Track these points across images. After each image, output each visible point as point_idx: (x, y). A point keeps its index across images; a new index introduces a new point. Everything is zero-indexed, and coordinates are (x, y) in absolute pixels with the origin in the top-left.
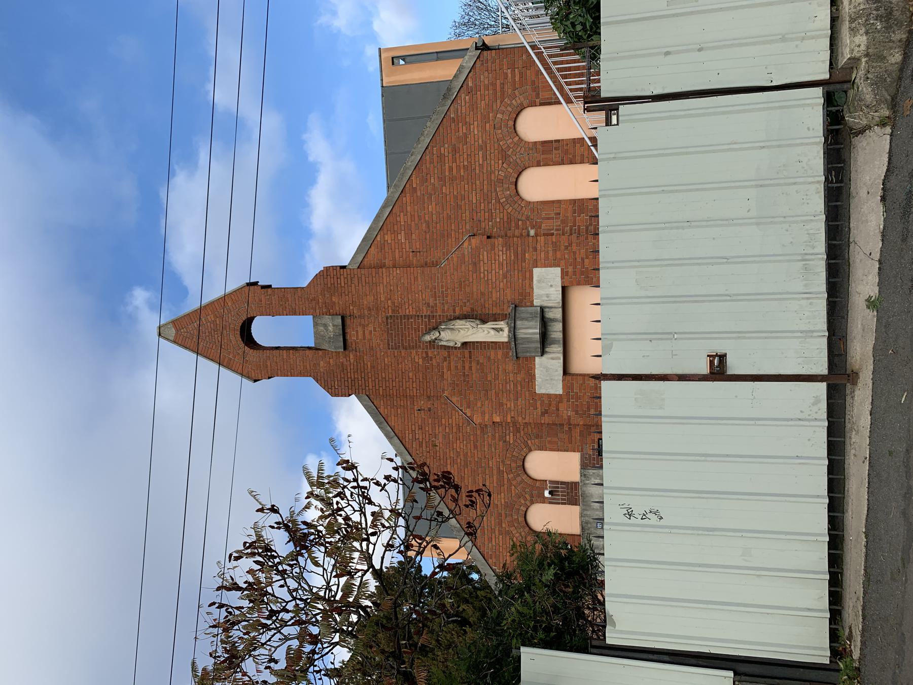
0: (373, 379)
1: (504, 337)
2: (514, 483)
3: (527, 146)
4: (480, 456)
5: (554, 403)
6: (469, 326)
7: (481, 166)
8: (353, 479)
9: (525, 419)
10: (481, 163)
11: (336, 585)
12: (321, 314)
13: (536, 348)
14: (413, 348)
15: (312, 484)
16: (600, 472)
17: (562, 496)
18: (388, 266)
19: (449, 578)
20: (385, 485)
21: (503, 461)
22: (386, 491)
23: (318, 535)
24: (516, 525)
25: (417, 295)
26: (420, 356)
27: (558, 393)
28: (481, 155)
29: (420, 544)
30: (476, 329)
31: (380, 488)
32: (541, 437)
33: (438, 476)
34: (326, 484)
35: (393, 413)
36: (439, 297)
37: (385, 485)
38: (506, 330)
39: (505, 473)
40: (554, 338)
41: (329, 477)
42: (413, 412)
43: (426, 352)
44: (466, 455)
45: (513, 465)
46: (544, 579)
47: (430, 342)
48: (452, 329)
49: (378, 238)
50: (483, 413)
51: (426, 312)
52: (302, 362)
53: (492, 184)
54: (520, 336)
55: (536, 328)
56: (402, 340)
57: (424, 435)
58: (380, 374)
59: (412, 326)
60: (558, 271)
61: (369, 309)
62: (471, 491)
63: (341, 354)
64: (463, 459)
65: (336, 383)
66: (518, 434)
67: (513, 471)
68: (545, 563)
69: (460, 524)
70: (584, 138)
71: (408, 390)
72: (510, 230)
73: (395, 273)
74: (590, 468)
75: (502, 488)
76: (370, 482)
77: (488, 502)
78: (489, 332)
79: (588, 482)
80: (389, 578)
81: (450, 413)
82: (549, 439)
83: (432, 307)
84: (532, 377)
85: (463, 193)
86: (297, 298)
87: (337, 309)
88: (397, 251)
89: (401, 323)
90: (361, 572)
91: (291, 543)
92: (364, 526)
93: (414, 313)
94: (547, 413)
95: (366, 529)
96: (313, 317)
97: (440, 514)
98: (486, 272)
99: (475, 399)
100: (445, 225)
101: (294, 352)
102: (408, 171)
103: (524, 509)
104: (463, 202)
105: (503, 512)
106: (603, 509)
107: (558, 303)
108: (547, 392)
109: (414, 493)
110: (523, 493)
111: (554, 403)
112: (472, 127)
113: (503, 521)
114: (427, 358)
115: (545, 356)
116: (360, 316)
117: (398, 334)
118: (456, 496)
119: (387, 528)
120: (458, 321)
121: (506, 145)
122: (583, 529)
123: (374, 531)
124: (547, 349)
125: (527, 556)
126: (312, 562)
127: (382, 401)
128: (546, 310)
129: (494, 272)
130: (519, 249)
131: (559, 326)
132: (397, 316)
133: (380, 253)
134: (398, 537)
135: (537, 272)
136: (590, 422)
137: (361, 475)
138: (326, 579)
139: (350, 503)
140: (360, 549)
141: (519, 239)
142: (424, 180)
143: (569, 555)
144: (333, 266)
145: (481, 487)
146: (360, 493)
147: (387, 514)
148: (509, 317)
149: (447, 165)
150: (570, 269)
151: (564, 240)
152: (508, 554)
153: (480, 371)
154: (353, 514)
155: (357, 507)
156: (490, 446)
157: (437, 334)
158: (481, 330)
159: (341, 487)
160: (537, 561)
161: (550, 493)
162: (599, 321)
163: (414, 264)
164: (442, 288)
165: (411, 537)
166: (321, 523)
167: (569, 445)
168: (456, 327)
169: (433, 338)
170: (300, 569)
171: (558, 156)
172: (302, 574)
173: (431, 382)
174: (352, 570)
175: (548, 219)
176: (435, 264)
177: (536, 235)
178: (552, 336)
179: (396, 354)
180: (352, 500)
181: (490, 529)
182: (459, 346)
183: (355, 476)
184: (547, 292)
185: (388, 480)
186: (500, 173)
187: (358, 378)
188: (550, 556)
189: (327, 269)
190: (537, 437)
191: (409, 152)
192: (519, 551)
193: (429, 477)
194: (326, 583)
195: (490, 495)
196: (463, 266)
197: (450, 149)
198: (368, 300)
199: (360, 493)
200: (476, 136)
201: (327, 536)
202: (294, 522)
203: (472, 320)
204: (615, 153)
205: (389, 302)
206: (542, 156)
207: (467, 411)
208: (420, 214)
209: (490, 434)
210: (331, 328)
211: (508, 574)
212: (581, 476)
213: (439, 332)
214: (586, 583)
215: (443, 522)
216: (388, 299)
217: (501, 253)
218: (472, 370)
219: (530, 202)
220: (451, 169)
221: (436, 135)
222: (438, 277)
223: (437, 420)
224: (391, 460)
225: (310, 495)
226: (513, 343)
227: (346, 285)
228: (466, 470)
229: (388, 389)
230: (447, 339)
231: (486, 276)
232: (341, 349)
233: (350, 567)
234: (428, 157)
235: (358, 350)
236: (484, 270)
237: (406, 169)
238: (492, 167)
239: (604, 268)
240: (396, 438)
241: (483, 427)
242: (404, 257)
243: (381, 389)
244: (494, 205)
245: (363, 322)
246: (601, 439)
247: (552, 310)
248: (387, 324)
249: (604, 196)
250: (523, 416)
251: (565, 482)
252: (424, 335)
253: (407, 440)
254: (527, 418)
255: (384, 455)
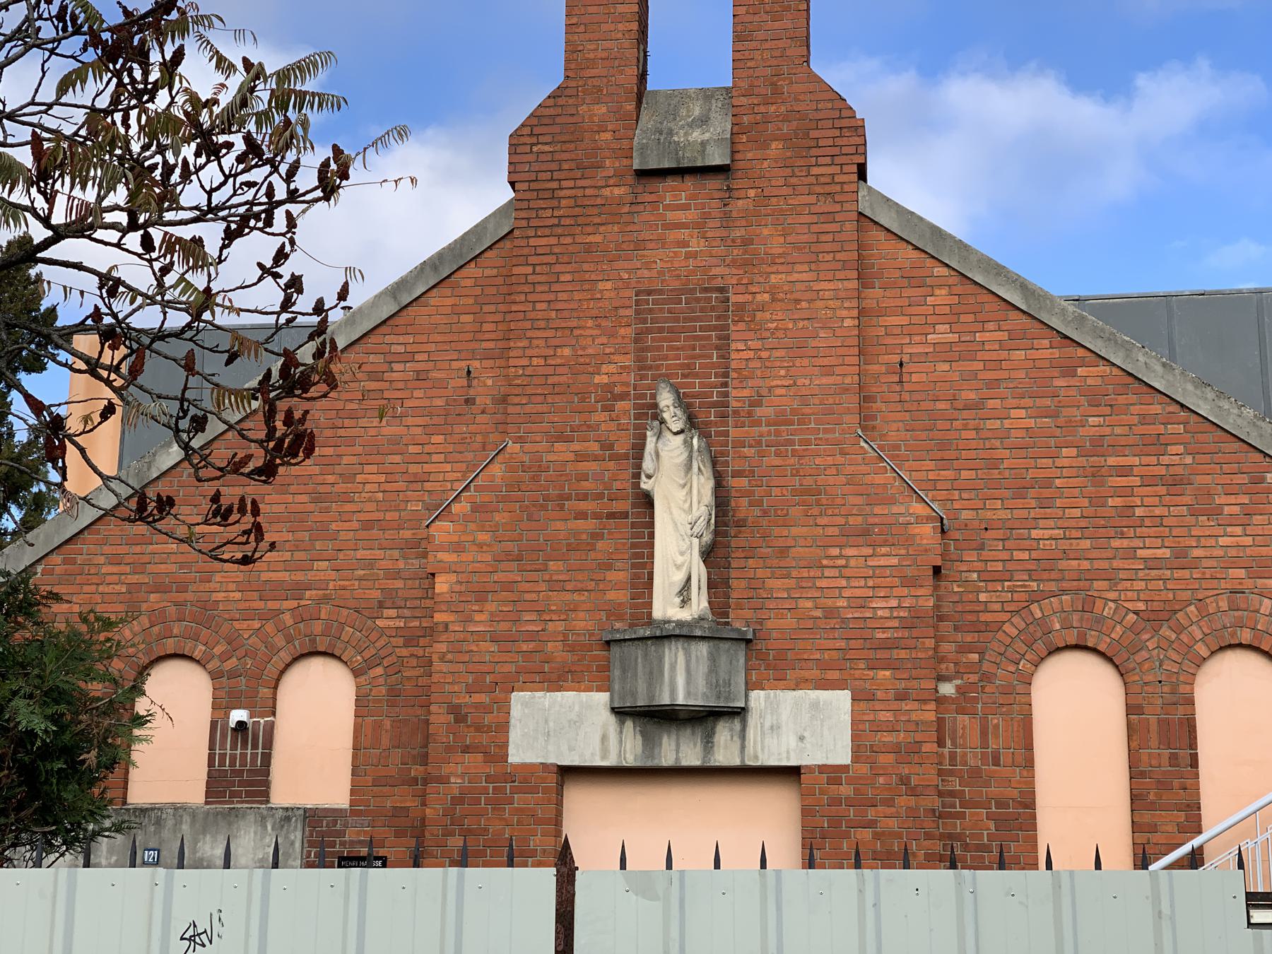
0: (556, 250)
1: (665, 607)
2: (270, 627)
3: (1181, 679)
4: (342, 535)
5: (484, 739)
6: (696, 513)
7: (1131, 553)
8: (296, 190)
9: (442, 659)
10: (1140, 553)
11: (5, 138)
12: (736, 111)
13: (634, 694)
14: (639, 359)
15: (283, 76)
16: (294, 860)
17: (233, 758)
18: (863, 296)
19: (11, 447)
20: (276, 276)
21: (326, 599)
22: (260, 280)
23: (145, 91)
24: (155, 630)
25: (783, 372)
26: (615, 378)
27: (511, 750)
28: (1160, 553)
29: (116, 369)
30: (689, 532)
31: (268, 264)
32: (392, 705)
33: (303, 420)
34: (285, 116)
35: (463, 301)
36: (778, 433)
37: (276, 276)
38: (685, 615)
39: (294, 604)
40: (661, 744)
41: (305, 124)
42: (463, 355)
43: (628, 394)
44: (346, 498)
45: (318, 627)
46: (18, 703)
47: (655, 406)
48: (689, 467)
49: (940, 271)
50: (458, 548)
51: (738, 395)
52: (604, 55)
53: (1082, 583)
54: (667, 651)
55: (688, 694)
56: (661, 330)
57: (401, 385)
58: (568, 268)
59: (701, 357)
60: (841, 755)
61: (746, 242)
62: (256, 512)
63: (625, 162)
64: (335, 489)
65: (547, 148)
66: (400, 641)
67: (301, 625)
68: (62, 708)
69: (158, 478)
70: (1200, 832)
71: (524, 343)
72: (956, 629)
73: (844, 313)
74: (307, 833)
75: (256, 595)
76: (283, 235)
77: (225, 557)
78: (678, 567)
79: (269, 828)
80: (11, 285)
81: (458, 457)
82: (387, 724)
83: (750, 414)
84: (555, 681)
85: (1058, 503)
86: (781, 44)
87: (749, 155)
88: (904, 320)
89: (710, 328)
90: (46, 206)
91: (121, 19)
92: (169, 216)
93: (733, 365)
94: (457, 721)
95: (161, 222)
96: (727, 89)
97: (199, 424)
98: (842, 562)
99: (497, 525)
100: (973, 454)
101: (635, 35)
102: (1121, 354)
103: (197, 655)
104: (1033, 503)
105: (189, 596)
106: (197, 868)
107: (756, 757)
108: (512, 721)
109: (256, 356)
110: (241, 652)
111: (484, 739)
112: (1239, 530)
113: (165, 596)
114: (610, 396)
115: (612, 720)
116: (727, 216)
117: (677, 320)
118: (246, 470)
119: (160, 284)
120: (711, 483)
121: (1184, 622)
122: (143, 811)
123: (157, 244)
124: (629, 724)
125: (82, 660)
126: (70, 73)
127: (495, 272)
128: (737, 724)
129: (844, 583)
130: (903, 654)
131: (691, 756)
132: (727, 317)
133: (898, 273)
134: (134, 311)
135: (840, 701)
136: (432, 835)
137: (304, 212)
138: (26, 110)
139: (231, 180)
140: (105, 204)
141: (931, 653)
142: (1095, 398)
143: (83, 773)
144: (865, 144)
145: (268, 538)
146: (256, 209)
147: (199, 280)
148: (718, 623)
149: (1136, 460)
150: (846, 790)
151: (925, 775)
152: (85, 609)
153: (573, 541)
154: (202, 186)
155: (217, 198)
156: (371, 563)
157: (676, 427)
158: (684, 546)
159: (276, 156)
160: (66, 687)
161: (241, 724)
162: (717, 865)
163: (868, 367)
164: (801, 442)
165: (135, 346)
166: (180, 99)
167: (370, 779)
168: (695, 478)
169: (666, 416)
170: (53, 41)
171: (1154, 762)
172: (38, 46)
173: (544, 408)
174: (50, 181)
175: (984, 734)
176: (867, 422)
177: (941, 701)
178: (665, 740)
179: (622, 312)
180: (237, 186)
181: (145, 559)
182: (643, 486)
183: (304, 194)
184: (784, 729)
185: (288, 286)
186: (1112, 605)
187: (559, 207)
188: (81, 722)
189: (859, 129)
190: (393, 693)
191: (1172, 357)
192: (95, 638)
193: (299, 396)
194: (14, 111)
195: (246, 560)
196: (859, 500)
197: (1179, 470)
198: (771, 240)
199: (256, 209)
200: (1212, 542)
201: (144, 118)
202: (181, 28)
203: (713, 521)
204: (1172, 918)
205: (766, 295)
206: (1153, 719)
207: (464, 503)
208: (1003, 385)
209: (401, 565)
210: (696, 135)
211: (31, 605)
212: (287, 809)
213: (681, 432)
214: (7, 817)
215: (177, 431)
216: (773, 294)
217: (894, 603)
218: (576, 518)
219: (1030, 684)
220: (1125, 471)
221: (1220, 433)
222: (833, 431)
223: (440, 420)
224: (343, 295)
225: (254, 71)
226: (648, 633)
227: (813, 180)
228: (305, 498)
229: (526, 289)
230: (661, 454)
231: (831, 563)
232: (641, 163)
233: (62, 176)
234: (1157, 409)
235: (635, 208)
236: (847, 558)
237: (1127, 349)
238: (1128, 584)
239: (862, 881)
240: (395, 309)
241: (420, 547)
242: (889, 340)
243: (529, 270)
244: (1021, 586)
245: (711, 223)
246: (384, 866)
247: (735, 738)
248: (706, 290)
249: (1057, 886)
250: (449, 656)
251: (269, 766)
252: (675, 390)
253: (388, 339)
254: (445, 667)
255: (357, 273)
